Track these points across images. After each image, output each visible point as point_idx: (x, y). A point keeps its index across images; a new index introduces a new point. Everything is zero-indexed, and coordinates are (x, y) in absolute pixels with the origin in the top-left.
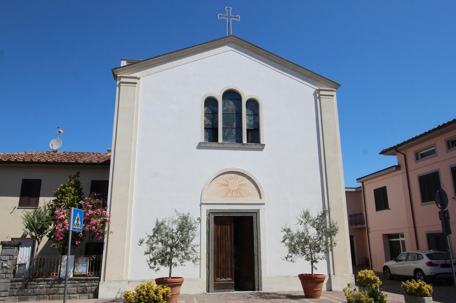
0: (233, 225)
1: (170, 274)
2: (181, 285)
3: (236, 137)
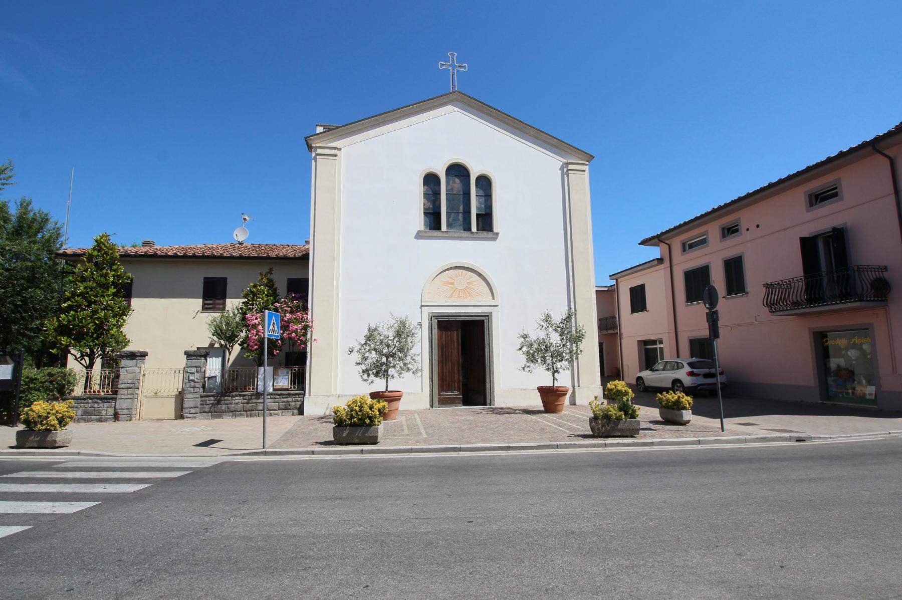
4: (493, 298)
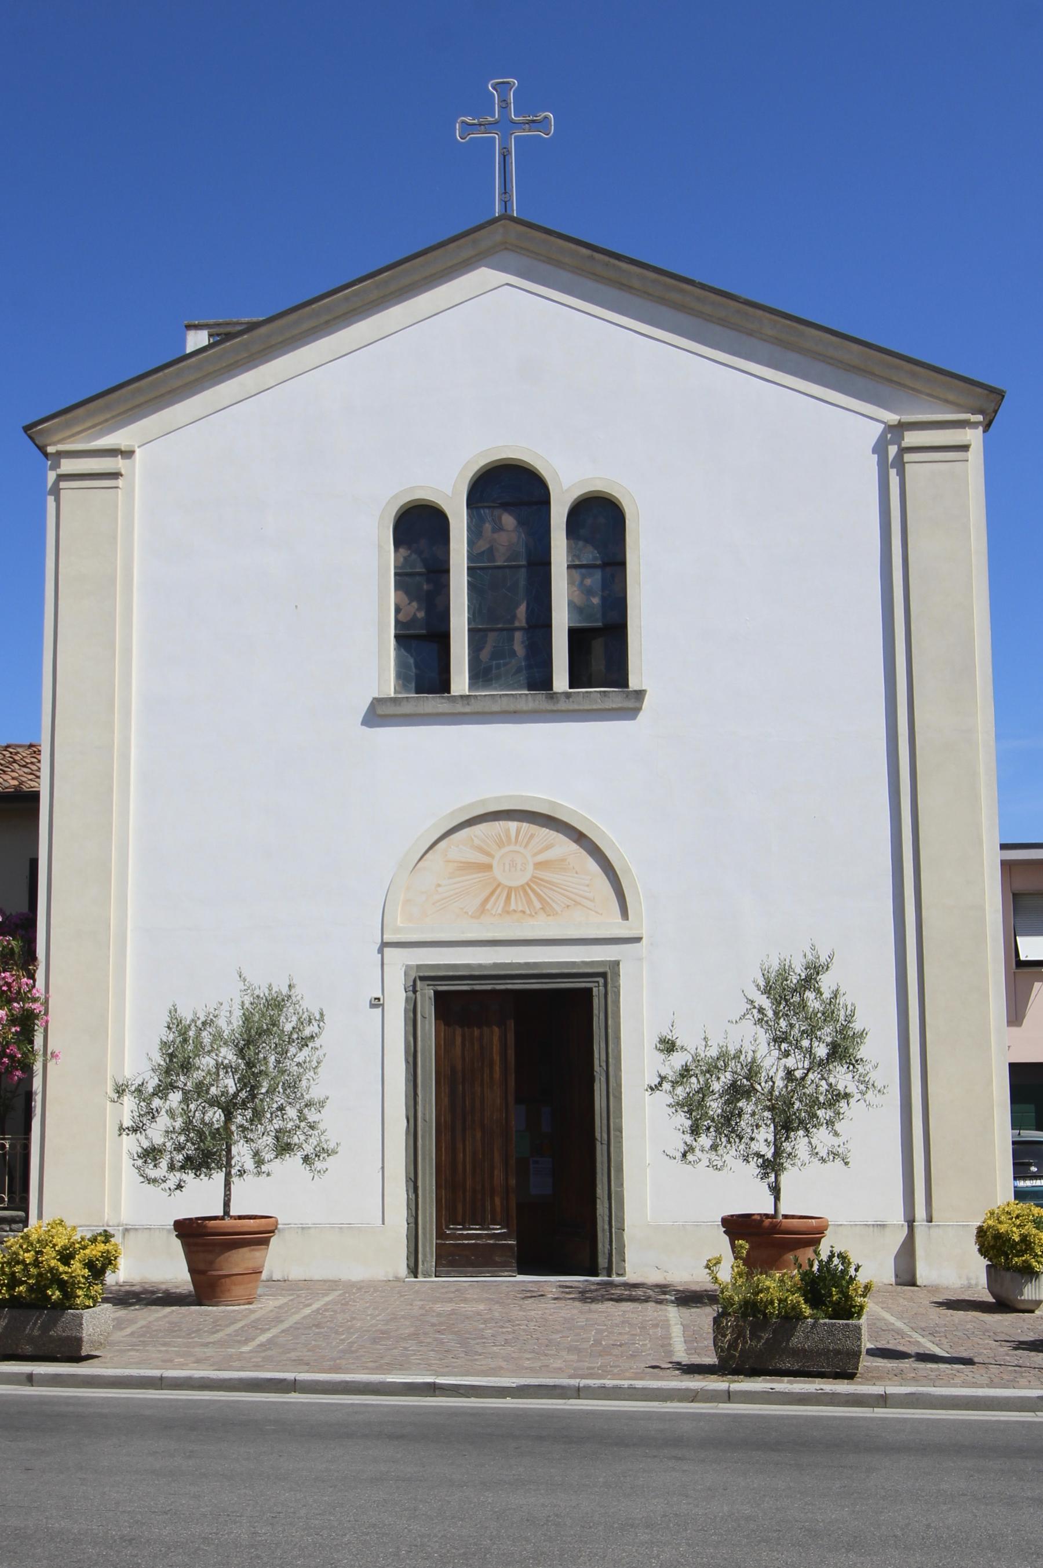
0: (511, 1024)
1: (227, 1204)
2: (265, 1242)
3: (529, 667)
4: (625, 913)
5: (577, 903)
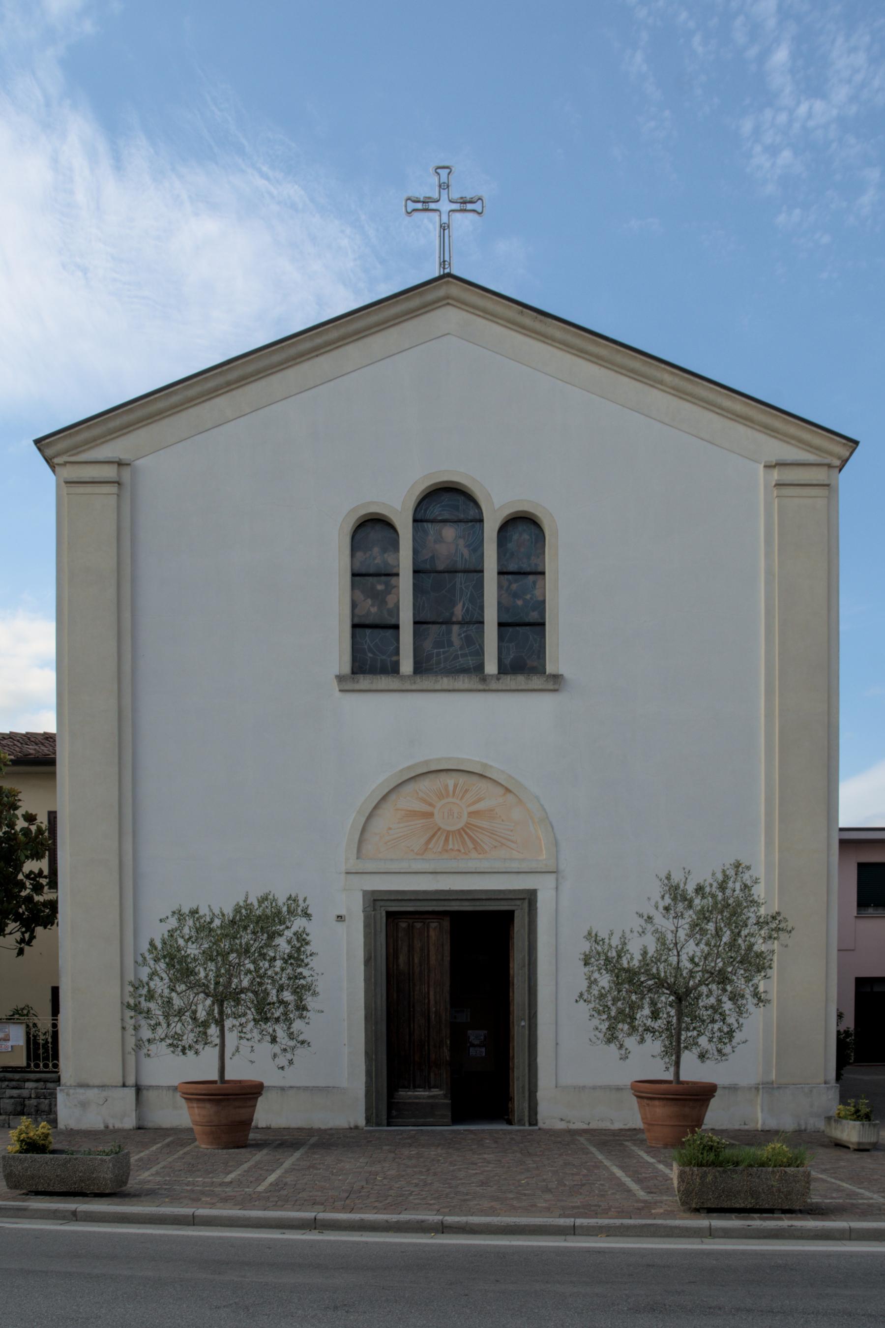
5: (503, 844)
